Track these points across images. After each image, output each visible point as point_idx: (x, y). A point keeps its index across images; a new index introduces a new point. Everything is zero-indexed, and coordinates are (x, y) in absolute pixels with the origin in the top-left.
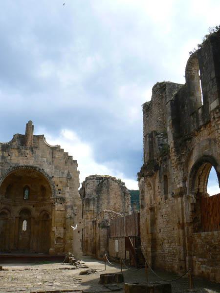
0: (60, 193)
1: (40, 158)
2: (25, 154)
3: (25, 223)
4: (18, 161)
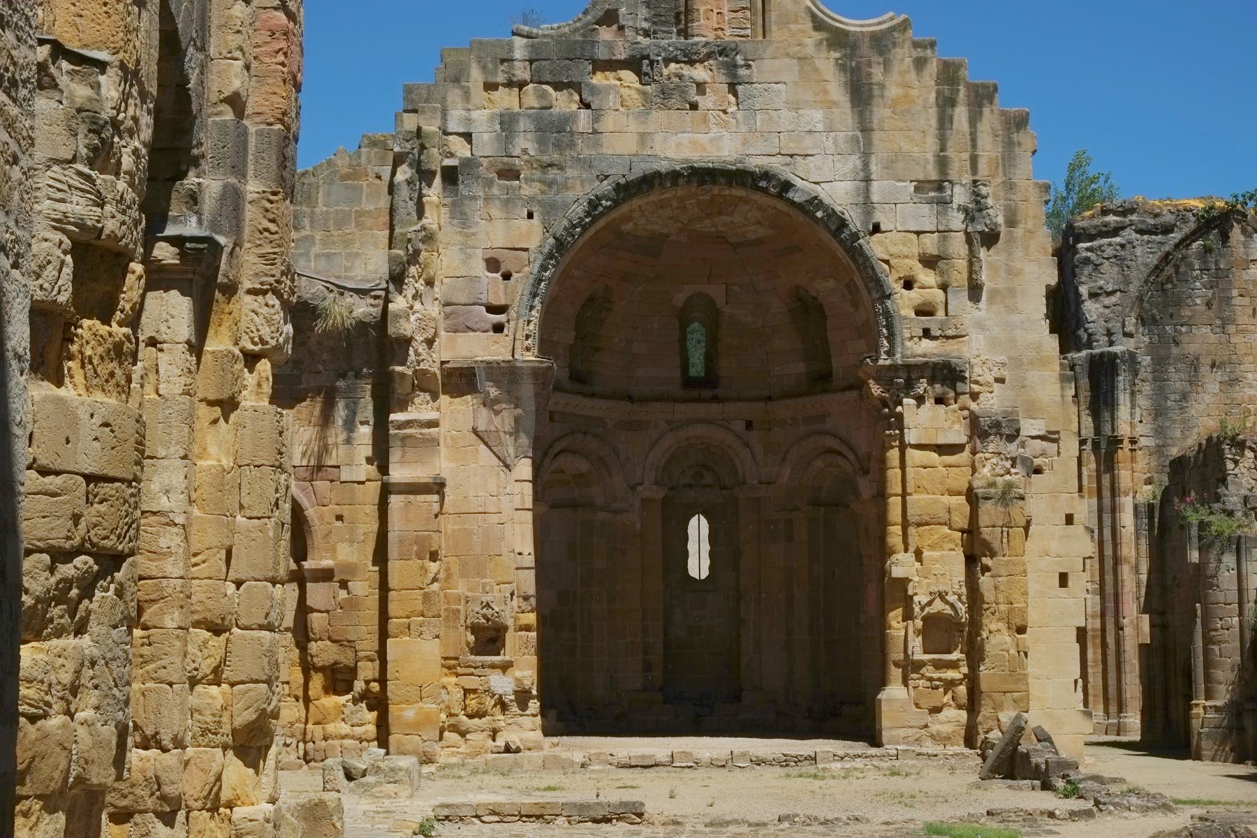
0: (927, 334)
1: (785, 114)
2: (683, 93)
3: (698, 529)
4: (643, 137)
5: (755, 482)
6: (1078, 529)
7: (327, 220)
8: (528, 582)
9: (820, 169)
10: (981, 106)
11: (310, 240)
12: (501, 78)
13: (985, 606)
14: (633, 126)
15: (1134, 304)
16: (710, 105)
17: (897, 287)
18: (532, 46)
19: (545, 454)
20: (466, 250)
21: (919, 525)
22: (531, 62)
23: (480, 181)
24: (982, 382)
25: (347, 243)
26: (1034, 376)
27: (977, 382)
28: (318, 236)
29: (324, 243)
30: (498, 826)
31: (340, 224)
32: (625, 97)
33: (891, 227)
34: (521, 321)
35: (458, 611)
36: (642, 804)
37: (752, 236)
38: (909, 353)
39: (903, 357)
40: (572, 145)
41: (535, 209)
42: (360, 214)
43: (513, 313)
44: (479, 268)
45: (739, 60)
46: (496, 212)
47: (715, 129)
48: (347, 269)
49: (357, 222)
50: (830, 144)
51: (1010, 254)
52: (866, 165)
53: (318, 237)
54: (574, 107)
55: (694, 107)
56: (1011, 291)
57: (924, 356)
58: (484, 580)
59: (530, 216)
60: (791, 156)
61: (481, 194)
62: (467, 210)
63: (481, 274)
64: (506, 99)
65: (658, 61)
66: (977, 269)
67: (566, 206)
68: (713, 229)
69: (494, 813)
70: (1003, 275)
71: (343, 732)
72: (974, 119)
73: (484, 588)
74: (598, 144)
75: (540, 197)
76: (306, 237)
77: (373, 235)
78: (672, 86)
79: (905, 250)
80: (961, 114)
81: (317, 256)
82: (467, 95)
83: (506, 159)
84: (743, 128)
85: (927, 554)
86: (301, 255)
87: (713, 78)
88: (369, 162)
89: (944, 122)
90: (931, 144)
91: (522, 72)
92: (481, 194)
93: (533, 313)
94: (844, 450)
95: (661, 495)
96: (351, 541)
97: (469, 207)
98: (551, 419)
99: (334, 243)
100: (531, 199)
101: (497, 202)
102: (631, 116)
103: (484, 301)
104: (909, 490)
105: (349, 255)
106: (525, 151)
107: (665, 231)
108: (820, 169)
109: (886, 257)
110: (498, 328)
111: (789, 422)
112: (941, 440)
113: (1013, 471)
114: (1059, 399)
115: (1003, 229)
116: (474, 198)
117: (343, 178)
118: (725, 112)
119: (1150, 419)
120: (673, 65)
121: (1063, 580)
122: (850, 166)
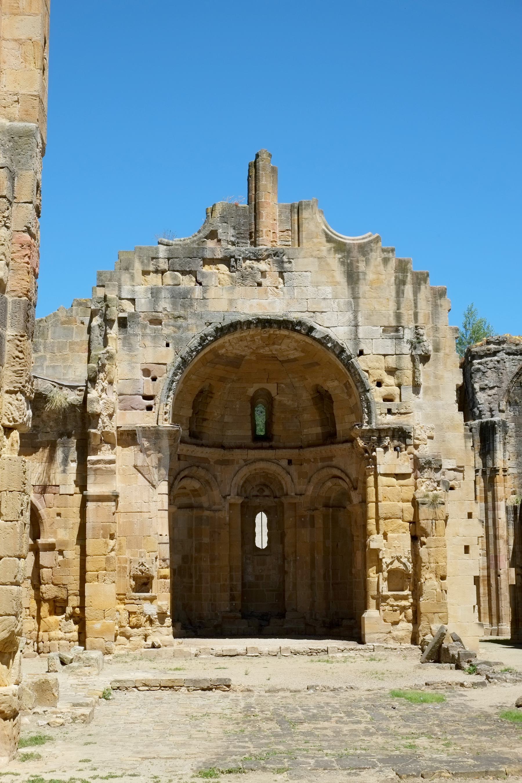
0: (389, 411)
2: (253, 277)
4: (231, 302)
5: (293, 494)
6: (475, 521)
7: (53, 347)
8: (165, 551)
9: (329, 319)
10: (420, 284)
11: (43, 358)
12: (152, 268)
13: (423, 564)
14: (226, 295)
15: (505, 394)
16: (269, 284)
17: (373, 386)
18: (169, 250)
19: (175, 478)
20: (131, 364)
21: (385, 519)
22: (169, 259)
23: (139, 325)
24: (421, 439)
25: (65, 360)
26: (449, 435)
27: (418, 439)
28: (48, 356)
29: (52, 360)
30: (148, 692)
31: (60, 350)
32: (221, 279)
33: (370, 352)
34: (162, 404)
35: (126, 567)
36: (230, 680)
37: (292, 357)
38: (379, 422)
39: (376, 424)
40: (191, 305)
41: (170, 341)
42: (72, 344)
43: (157, 400)
44: (139, 374)
45: (285, 259)
46: (148, 342)
47: (271, 297)
48: (64, 374)
49: (70, 348)
50: (335, 305)
51: (436, 367)
52: (356, 317)
53: (48, 356)
54: (193, 284)
55: (259, 285)
56: (437, 388)
57: (388, 424)
58: (141, 550)
59: (168, 345)
60: (314, 312)
61: (140, 333)
62: (132, 342)
63: (139, 378)
64: (154, 280)
65: (239, 259)
66: (418, 375)
67: (188, 340)
68: (270, 353)
69: (145, 685)
70: (432, 378)
71: (60, 636)
72: (416, 293)
73: (140, 555)
74: (205, 305)
75: (173, 335)
76: (41, 356)
77: (79, 355)
78: (247, 273)
79: (377, 365)
80: (408, 289)
81: (47, 367)
82: (132, 277)
83: (154, 313)
84: (287, 297)
85: (390, 535)
86: (38, 366)
87: (270, 268)
88: (77, 314)
89: (399, 293)
90: (392, 306)
91: (163, 265)
92: (140, 333)
93: (169, 399)
94: (343, 476)
95: (240, 501)
96: (66, 528)
97: (133, 340)
98: (179, 459)
99: (57, 360)
100: (168, 336)
101: (149, 337)
102: (224, 290)
103: (141, 393)
104: (380, 499)
105: (65, 367)
106: (165, 309)
107: (243, 354)
108: (329, 319)
109: (367, 369)
110: (149, 408)
111: (312, 460)
112: (397, 471)
113: (438, 488)
114: (464, 448)
115: (432, 353)
116: (136, 335)
117: (63, 323)
118: (277, 288)
119: (514, 458)
120: (248, 262)
121: (467, 549)
122: (347, 318)
